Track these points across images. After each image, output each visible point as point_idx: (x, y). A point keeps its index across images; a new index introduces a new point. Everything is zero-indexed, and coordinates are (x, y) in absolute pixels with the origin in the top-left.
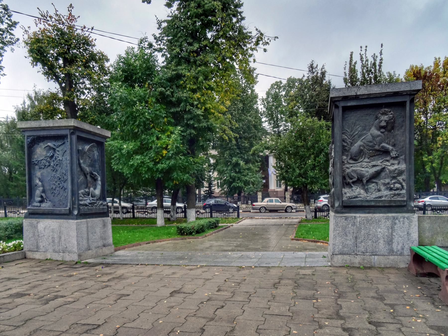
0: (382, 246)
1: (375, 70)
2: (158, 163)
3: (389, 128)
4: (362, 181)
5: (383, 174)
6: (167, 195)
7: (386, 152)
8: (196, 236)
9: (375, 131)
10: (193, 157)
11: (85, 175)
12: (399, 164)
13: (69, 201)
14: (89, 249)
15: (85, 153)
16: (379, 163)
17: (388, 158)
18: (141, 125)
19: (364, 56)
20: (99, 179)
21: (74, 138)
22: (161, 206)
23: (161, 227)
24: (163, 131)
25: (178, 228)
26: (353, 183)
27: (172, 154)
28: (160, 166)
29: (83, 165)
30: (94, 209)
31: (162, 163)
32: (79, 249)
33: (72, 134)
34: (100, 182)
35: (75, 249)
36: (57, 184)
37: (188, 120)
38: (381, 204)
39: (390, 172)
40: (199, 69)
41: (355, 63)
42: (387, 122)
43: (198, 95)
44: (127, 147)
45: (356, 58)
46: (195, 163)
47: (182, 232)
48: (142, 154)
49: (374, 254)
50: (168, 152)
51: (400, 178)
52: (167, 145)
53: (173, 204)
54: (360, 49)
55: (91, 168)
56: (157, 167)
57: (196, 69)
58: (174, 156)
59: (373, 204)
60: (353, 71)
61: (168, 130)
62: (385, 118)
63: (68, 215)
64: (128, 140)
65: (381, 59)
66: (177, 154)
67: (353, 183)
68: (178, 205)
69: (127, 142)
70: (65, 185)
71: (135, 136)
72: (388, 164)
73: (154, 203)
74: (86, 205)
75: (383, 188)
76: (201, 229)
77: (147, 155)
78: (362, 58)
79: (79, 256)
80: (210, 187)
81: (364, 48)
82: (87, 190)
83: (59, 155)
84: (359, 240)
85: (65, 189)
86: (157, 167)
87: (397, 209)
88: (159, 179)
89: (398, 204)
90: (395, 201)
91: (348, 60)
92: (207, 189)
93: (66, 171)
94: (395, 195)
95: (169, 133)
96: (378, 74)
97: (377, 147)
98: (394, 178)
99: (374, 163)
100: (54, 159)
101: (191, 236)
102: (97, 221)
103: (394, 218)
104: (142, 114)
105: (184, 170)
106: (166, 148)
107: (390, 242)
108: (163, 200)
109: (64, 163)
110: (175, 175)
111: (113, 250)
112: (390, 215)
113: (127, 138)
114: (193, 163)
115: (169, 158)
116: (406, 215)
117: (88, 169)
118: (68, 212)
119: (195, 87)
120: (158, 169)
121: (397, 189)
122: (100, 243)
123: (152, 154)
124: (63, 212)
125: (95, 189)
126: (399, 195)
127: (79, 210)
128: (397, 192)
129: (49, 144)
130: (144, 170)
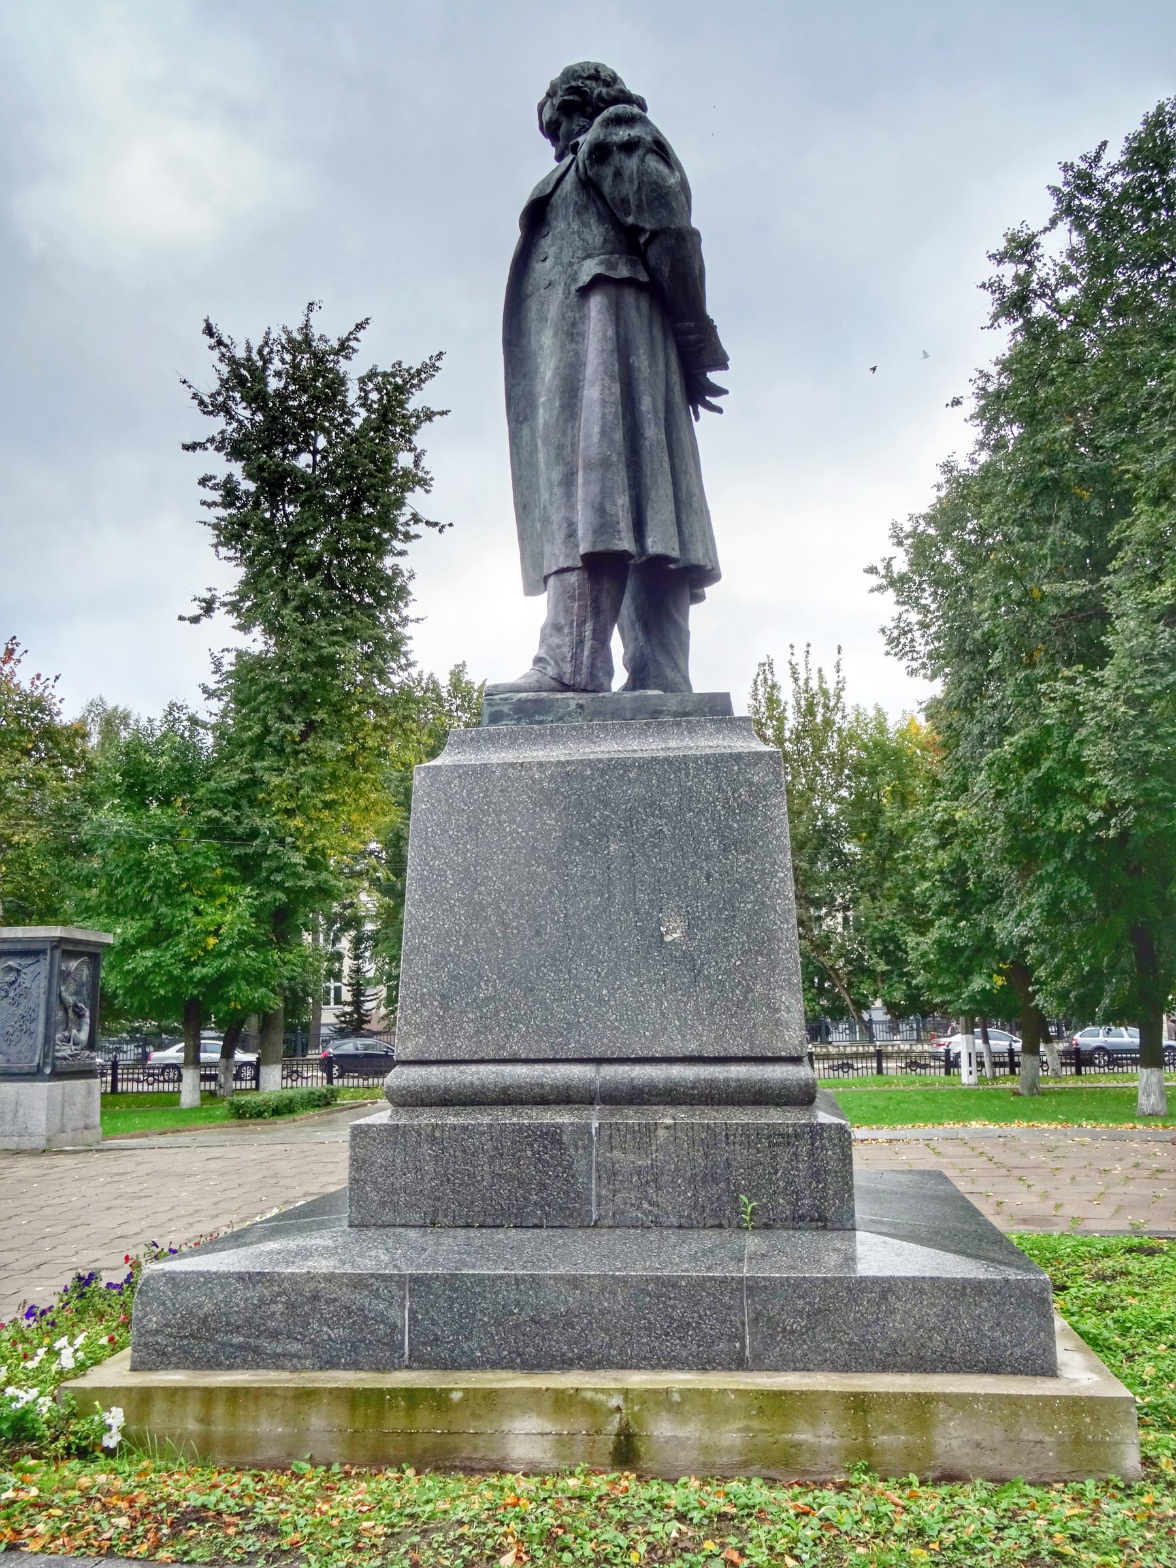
2: (195, 964)
6: (212, 1029)
8: (271, 1120)
10: (281, 950)
11: (66, 1010)
13: (38, 1052)
14: (62, 1130)
15: (69, 973)
18: (159, 887)
19: (801, 669)
20: (88, 1014)
21: (58, 953)
22: (193, 1059)
23: (192, 1109)
24: (211, 896)
25: (232, 1104)
27: (230, 947)
28: (198, 972)
29: (64, 994)
30: (75, 1064)
31: (204, 966)
32: (48, 1129)
33: (54, 948)
34: (88, 1020)
35: (42, 1129)
36: (17, 1026)
37: (271, 871)
40: (303, 769)
43: (298, 822)
44: (123, 933)
45: (782, 677)
46: (285, 963)
47: (242, 1114)
48: (156, 945)
50: (221, 941)
52: (219, 927)
53: (227, 1053)
54: (789, 650)
55: (75, 998)
56: (190, 973)
57: (296, 768)
58: (233, 950)
61: (224, 892)
63: (34, 1075)
64: (124, 914)
66: (240, 946)
68: (240, 1056)
69: (122, 920)
70: (32, 1027)
71: (142, 907)
73: (174, 1054)
74: (65, 1058)
76: (285, 1106)
77: (167, 948)
79: (49, 1140)
80: (357, 1003)
82: (66, 1034)
83: (26, 980)
85: (32, 1033)
86: (190, 973)
88: (194, 999)
92: (348, 1009)
93: (38, 1005)
95: (225, 900)
100: (16, 985)
101: (260, 1120)
102: (79, 1085)
104: (164, 865)
105: (257, 978)
106: (216, 933)
108: (200, 1044)
109: (34, 992)
110: (232, 990)
111: (99, 1137)
113: (121, 908)
114: (280, 963)
115: (222, 955)
117: (71, 1000)
118: (35, 1070)
119: (291, 805)
120: (191, 978)
122: (81, 1124)
123: (182, 948)
124: (26, 1070)
125: (79, 1031)
127: (54, 1067)
129: (10, 963)
130: (156, 980)
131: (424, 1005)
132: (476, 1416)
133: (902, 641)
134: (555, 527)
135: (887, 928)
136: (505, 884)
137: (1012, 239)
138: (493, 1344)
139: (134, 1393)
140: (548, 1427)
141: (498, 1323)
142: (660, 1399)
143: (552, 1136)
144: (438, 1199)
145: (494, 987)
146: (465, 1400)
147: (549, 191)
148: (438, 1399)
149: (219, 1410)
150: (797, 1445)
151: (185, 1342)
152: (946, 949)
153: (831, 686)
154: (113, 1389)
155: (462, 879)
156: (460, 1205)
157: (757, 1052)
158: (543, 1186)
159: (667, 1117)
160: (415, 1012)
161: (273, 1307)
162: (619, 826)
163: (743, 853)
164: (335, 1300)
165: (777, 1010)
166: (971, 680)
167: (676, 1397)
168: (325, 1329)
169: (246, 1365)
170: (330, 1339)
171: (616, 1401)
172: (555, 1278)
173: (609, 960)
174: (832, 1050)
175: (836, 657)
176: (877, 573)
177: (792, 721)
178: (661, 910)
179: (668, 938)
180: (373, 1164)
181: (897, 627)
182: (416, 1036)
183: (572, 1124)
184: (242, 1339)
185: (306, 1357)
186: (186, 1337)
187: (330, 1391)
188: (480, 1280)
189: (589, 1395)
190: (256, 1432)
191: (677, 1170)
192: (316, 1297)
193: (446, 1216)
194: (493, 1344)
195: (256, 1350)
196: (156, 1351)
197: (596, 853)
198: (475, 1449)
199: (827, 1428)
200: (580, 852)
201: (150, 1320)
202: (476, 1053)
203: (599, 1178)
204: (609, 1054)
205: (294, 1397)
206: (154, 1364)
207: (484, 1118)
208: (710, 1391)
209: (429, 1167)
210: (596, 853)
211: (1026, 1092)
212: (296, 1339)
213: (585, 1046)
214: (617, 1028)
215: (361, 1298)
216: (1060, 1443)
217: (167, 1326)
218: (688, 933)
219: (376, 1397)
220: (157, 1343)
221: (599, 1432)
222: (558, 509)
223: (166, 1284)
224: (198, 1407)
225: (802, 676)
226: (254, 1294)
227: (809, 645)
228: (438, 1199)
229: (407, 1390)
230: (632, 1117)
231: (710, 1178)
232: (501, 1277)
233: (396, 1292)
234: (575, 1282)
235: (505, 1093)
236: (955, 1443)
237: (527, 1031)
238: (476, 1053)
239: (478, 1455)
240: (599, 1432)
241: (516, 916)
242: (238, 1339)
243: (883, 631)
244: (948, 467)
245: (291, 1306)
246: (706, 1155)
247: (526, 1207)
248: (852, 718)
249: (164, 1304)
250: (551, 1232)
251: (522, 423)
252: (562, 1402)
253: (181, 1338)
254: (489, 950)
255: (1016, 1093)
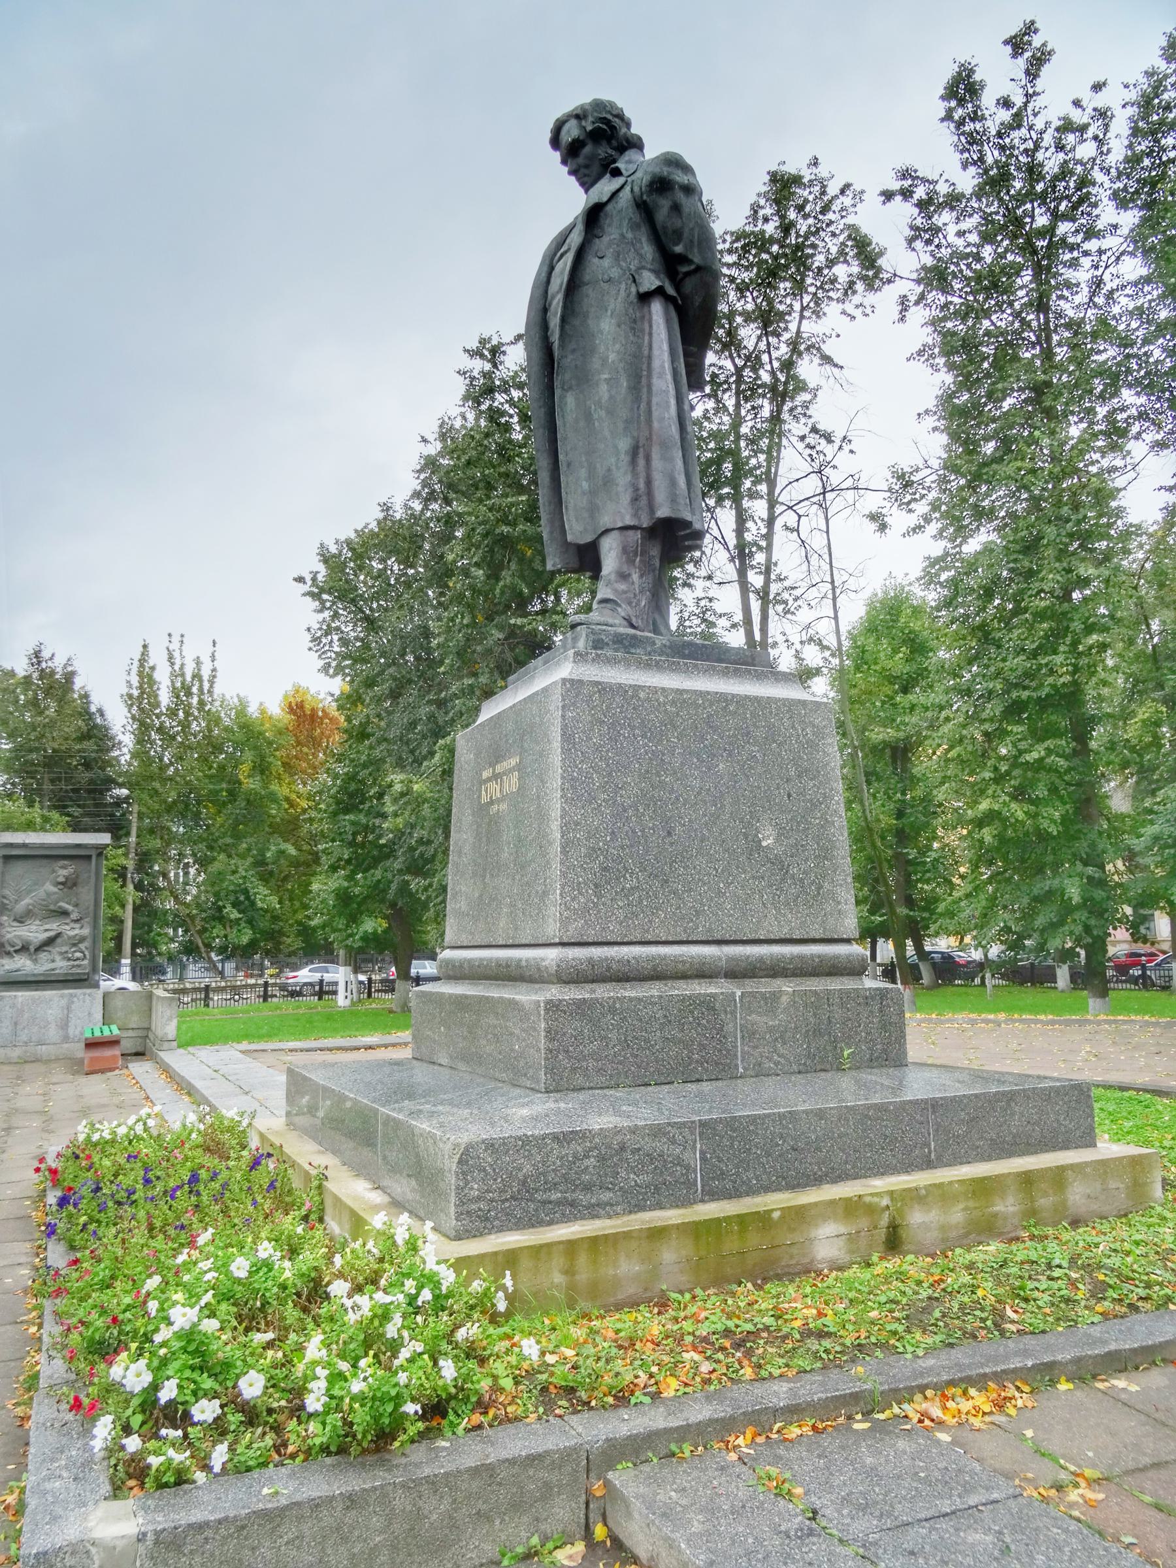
0: (53, 1033)
1: (201, 689)
3: (69, 884)
4: (28, 949)
5: (59, 940)
7: (65, 913)
9: (50, 887)
12: (81, 928)
16: (54, 926)
17: (68, 921)
19: (176, 654)
26: (16, 951)
38: (53, 978)
39: (70, 938)
41: (153, 668)
42: (67, 878)
45: (158, 658)
49: (41, 1043)
51: (82, 946)
54: (167, 638)
59: (42, 978)
60: (147, 678)
62: (65, 872)
65: (214, 670)
67: (16, 951)
72: (67, 927)
75: (58, 958)
78: (171, 658)
81: (176, 639)
84: (19, 1027)
87: (74, 984)
89: (77, 977)
90: (72, 974)
91: (137, 656)
94: (73, 966)
96: (206, 697)
97: (52, 907)
98: (74, 945)
99: (47, 927)
103: (71, 995)
107: (64, 1025)
112: (66, 992)
116: (88, 991)
121: (78, 959)
126: (79, 966)
128: (77, 963)
131: (580, 893)
132: (792, 1230)
133: (324, 640)
134: (620, 489)
135: (241, 881)
136: (642, 790)
137: (483, 342)
138: (765, 1172)
139: (500, 1258)
140: (842, 1229)
141: (768, 1154)
142: (914, 1196)
143: (707, 1004)
144: (620, 1063)
145: (637, 879)
146: (782, 1217)
147: (605, 199)
148: (762, 1219)
149: (582, 1260)
150: (995, 1215)
151: (507, 1204)
152: (344, 898)
153: (206, 673)
154: (478, 1256)
155: (607, 782)
156: (639, 1067)
157: (828, 935)
158: (702, 1047)
159: (787, 987)
160: (573, 899)
161: (587, 1162)
162: (725, 750)
163: (812, 779)
164: (639, 1149)
165: (839, 903)
166: (395, 679)
167: (923, 1192)
168: (632, 1176)
169: (566, 1219)
170: (637, 1185)
171: (885, 1202)
172: (806, 1112)
173: (723, 859)
174: (188, 986)
175: (212, 649)
176: (305, 583)
177: (165, 698)
178: (758, 821)
179: (764, 844)
180: (564, 1034)
181: (320, 629)
182: (575, 920)
183: (722, 993)
184: (559, 1195)
185: (617, 1204)
186: (507, 1200)
187: (678, 1226)
188: (753, 1119)
189: (868, 1199)
190: (616, 1275)
191: (796, 1028)
192: (623, 1148)
193: (627, 1077)
194: (765, 1172)
195: (573, 1204)
196: (479, 1217)
197: (709, 769)
198: (792, 1257)
199: (1011, 1200)
200: (697, 768)
201: (472, 1189)
202: (626, 936)
203: (743, 1037)
204: (727, 937)
205: (648, 1237)
206: (478, 1230)
207: (653, 990)
208: (942, 1184)
209: (613, 1036)
210: (709, 769)
211: (399, 1010)
212: (608, 1189)
213: (710, 930)
214: (732, 915)
215: (661, 1145)
216: (1127, 1188)
217: (488, 1191)
218: (777, 840)
219: (713, 1227)
220: (480, 1209)
221: (875, 1227)
222: (625, 473)
223: (485, 1150)
224: (562, 1260)
225: (178, 662)
226: (568, 1151)
227: (182, 636)
228: (620, 1063)
229: (738, 1216)
230: (766, 986)
231: (818, 1033)
232: (769, 1115)
233: (689, 1137)
234: (821, 1114)
235: (655, 970)
236: (1077, 1197)
237: (665, 917)
238: (626, 936)
239: (793, 1262)
240: (875, 1227)
241: (651, 818)
242: (555, 1196)
243: (309, 629)
244: (386, 508)
245: (602, 1159)
246: (815, 1015)
247: (690, 1064)
248: (217, 704)
249: (484, 1170)
250: (658, 1088)
251: (567, 391)
252: (851, 1208)
253: (503, 1202)
254: (632, 846)
255: (391, 1011)
